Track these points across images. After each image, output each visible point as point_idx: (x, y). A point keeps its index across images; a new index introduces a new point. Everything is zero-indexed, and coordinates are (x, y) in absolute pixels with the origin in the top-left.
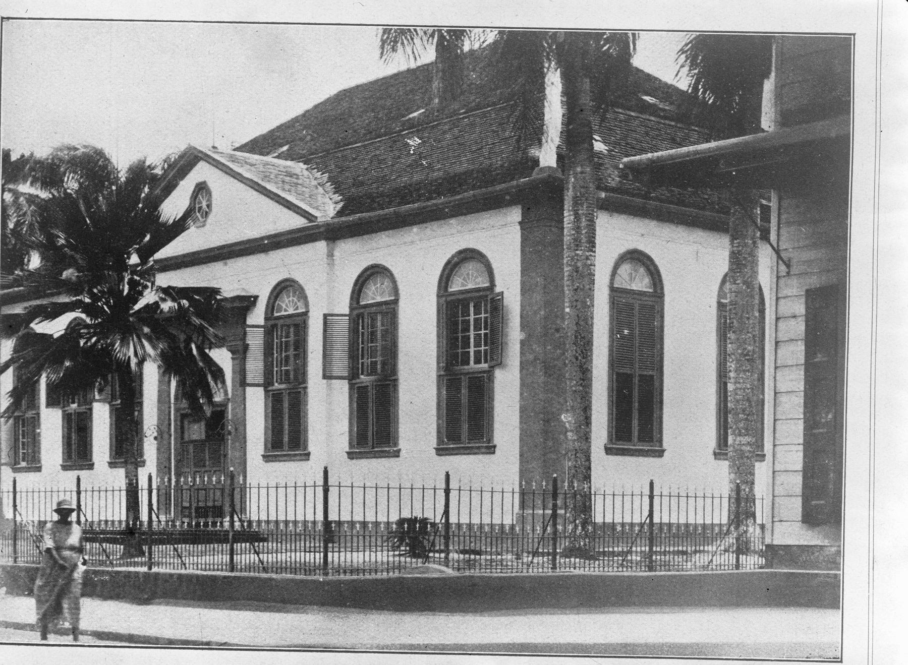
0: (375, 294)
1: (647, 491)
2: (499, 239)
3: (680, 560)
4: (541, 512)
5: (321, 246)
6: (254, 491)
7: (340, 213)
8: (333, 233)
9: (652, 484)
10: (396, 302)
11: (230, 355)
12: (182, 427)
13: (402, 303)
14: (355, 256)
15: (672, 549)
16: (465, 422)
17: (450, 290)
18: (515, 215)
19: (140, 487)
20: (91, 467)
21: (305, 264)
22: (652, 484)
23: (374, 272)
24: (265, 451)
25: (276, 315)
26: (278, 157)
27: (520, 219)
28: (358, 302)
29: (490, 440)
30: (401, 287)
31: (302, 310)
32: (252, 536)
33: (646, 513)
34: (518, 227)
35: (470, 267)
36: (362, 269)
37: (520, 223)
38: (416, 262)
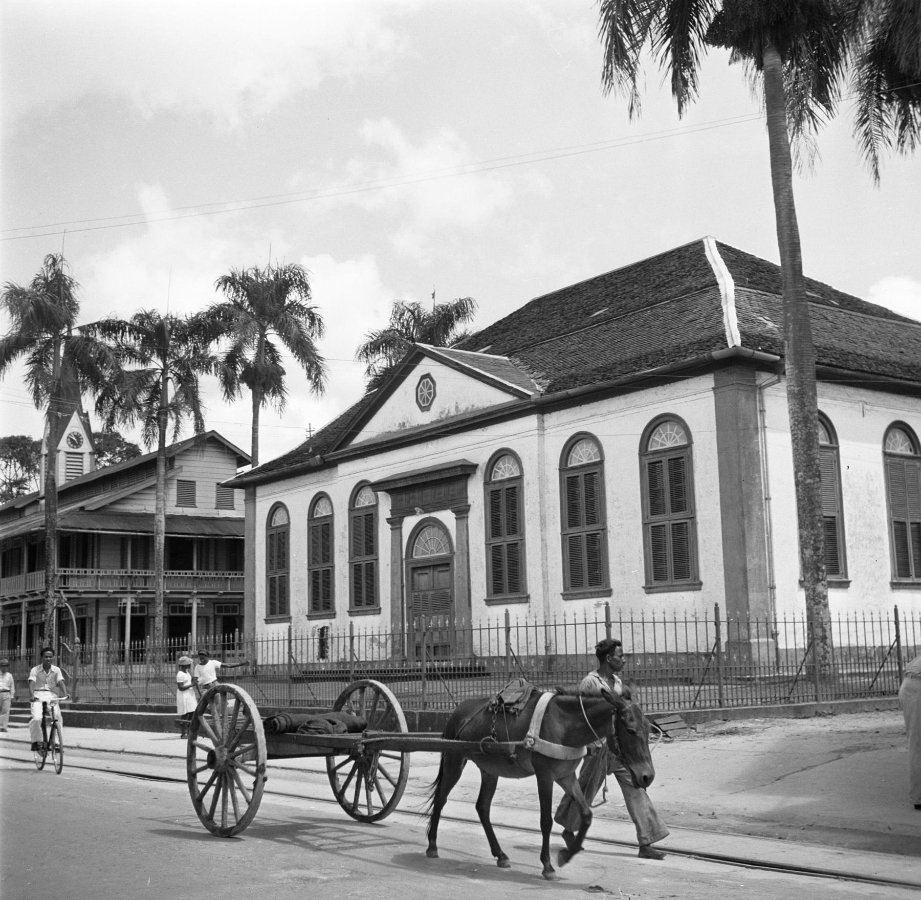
0: (583, 455)
1: (892, 618)
2: (695, 403)
3: (463, 684)
4: (761, 640)
5: (532, 421)
6: (260, 644)
7: (549, 390)
8: (543, 408)
9: (896, 610)
10: (601, 463)
11: (454, 515)
12: (413, 577)
13: (695, 447)
14: (564, 424)
15: (845, 672)
16: (671, 561)
17: (650, 449)
18: (707, 382)
19: (475, 625)
20: (333, 615)
21: (520, 434)
22: (896, 610)
23: (321, 496)
24: (488, 596)
25: (569, 466)
26: (485, 352)
27: (713, 385)
28: (566, 465)
29: (525, 592)
30: (605, 449)
31: (517, 474)
32: (476, 671)
33: (893, 638)
34: (712, 393)
35: (322, 503)
36: (567, 438)
37: (713, 389)
38: (617, 429)
